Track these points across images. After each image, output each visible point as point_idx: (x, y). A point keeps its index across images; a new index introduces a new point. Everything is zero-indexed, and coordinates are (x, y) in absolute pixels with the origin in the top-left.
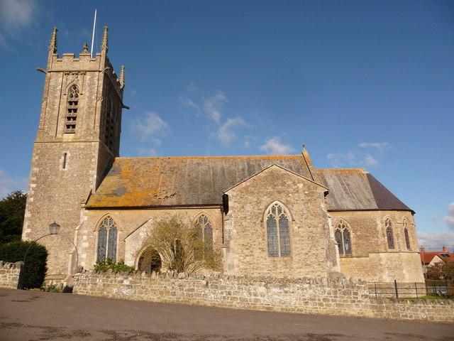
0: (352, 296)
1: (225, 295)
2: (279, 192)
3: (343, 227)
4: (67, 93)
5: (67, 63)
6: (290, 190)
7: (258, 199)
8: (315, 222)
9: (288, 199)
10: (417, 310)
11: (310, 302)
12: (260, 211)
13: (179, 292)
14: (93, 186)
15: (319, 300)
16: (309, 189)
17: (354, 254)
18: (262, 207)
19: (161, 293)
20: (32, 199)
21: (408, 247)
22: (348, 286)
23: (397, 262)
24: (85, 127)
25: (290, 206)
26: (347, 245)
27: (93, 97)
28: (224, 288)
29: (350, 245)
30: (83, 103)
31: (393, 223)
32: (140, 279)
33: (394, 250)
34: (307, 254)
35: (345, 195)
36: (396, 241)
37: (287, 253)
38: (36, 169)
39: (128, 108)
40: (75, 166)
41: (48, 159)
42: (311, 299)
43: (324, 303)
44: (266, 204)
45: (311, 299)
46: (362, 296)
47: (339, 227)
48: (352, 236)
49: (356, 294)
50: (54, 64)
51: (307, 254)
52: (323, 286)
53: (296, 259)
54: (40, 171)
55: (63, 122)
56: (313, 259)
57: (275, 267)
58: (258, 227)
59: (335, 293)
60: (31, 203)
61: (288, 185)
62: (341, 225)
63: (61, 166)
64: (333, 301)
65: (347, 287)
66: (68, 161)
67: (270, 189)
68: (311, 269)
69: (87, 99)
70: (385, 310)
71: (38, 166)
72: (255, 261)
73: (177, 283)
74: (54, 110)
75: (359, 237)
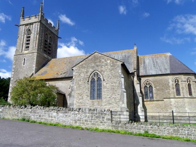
0: (101, 119)
1: (38, 117)
2: (97, 66)
3: (149, 84)
4: (26, 33)
5: (27, 21)
6: (103, 64)
7: (87, 70)
8: (115, 80)
9: (102, 69)
10: (140, 129)
11: (78, 121)
12: (87, 76)
13: (19, 115)
14: (34, 72)
15: (83, 121)
16: (113, 63)
17: (155, 99)
18: (89, 74)
19: (13, 115)
20: (12, 79)
21: (190, 94)
22: (99, 113)
23: (182, 103)
24: (32, 46)
25: (103, 73)
26: (151, 95)
27: (36, 33)
28: (38, 113)
29: (152, 94)
30: (32, 36)
31: (180, 81)
32: (6, 109)
33: (180, 97)
34: (110, 98)
35: (153, 67)
36: (181, 91)
37: (99, 96)
38: (14, 66)
39: (61, 38)
40: (28, 63)
41: (18, 62)
42: (78, 120)
43: (85, 123)
44: (91, 73)
45: (78, 120)
46: (107, 119)
47: (147, 84)
48: (153, 89)
49: (103, 118)
50: (22, 22)
51: (110, 98)
52: (86, 113)
53: (104, 100)
54: (16, 67)
55: (24, 45)
56: (113, 101)
57: (93, 104)
58: (86, 85)
59: (92, 117)
60: (12, 80)
61: (103, 62)
62: (148, 83)
63: (23, 64)
64: (90, 121)
65: (98, 114)
66: (25, 62)
67: (93, 65)
68: (112, 106)
69: (33, 35)
70: (120, 128)
71: (15, 65)
72: (84, 102)
73: (19, 110)
74: (21, 41)
75: (158, 90)
